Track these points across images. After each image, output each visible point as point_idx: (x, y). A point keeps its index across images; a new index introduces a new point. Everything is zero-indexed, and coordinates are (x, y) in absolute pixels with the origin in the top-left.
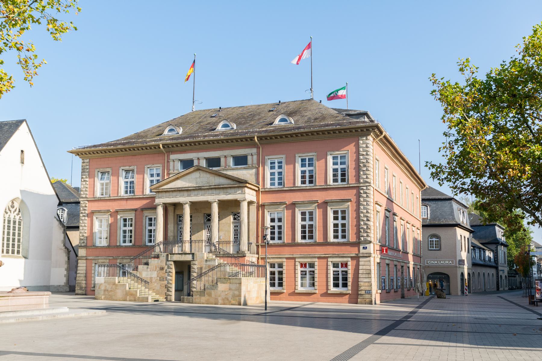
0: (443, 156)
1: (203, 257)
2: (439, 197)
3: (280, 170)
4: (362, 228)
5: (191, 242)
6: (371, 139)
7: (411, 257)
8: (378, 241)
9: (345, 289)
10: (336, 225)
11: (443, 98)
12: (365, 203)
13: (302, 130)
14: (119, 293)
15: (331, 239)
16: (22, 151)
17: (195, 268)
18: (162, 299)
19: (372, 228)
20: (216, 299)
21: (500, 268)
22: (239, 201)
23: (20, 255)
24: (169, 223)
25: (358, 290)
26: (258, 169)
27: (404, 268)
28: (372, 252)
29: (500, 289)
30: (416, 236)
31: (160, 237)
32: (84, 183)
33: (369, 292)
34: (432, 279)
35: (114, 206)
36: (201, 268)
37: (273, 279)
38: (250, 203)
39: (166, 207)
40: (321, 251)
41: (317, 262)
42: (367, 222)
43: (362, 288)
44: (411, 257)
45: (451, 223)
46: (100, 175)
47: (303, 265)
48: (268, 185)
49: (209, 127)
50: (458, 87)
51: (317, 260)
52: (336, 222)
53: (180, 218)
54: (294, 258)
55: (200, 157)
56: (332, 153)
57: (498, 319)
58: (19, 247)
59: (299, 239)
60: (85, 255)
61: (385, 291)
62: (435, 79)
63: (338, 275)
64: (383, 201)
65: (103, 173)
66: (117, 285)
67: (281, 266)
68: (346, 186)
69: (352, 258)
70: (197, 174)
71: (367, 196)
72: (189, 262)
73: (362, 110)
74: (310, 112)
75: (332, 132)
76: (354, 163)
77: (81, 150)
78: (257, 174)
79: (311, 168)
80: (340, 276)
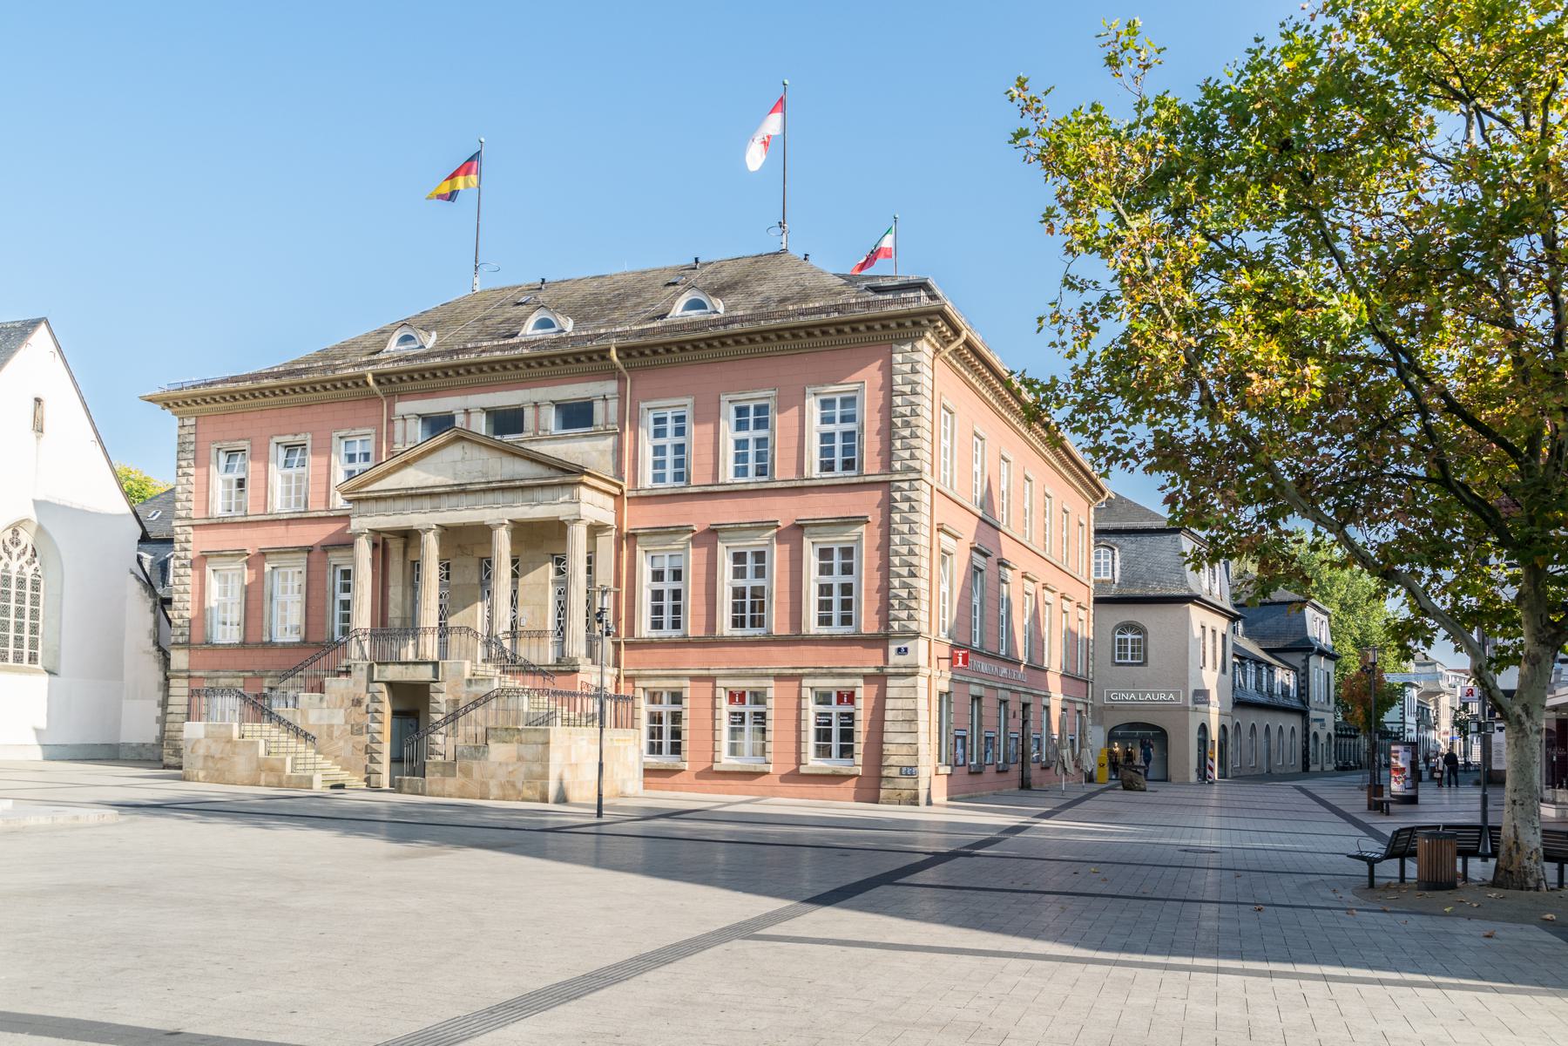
0: (1053, 345)
1: (464, 670)
2: (1147, 524)
3: (679, 440)
4: (896, 596)
5: (444, 630)
6: (929, 350)
7: (1054, 683)
8: (943, 635)
9: (846, 761)
10: (825, 590)
11: (1053, 158)
12: (905, 528)
13: (736, 327)
14: (242, 766)
15: (812, 626)
16: (38, 400)
17: (441, 702)
18: (355, 780)
19: (925, 596)
20: (484, 784)
21: (1313, 714)
22: (562, 523)
23: (39, 666)
24: (391, 583)
25: (880, 766)
26: (620, 436)
27: (1032, 708)
28: (922, 660)
29: (1313, 768)
30: (1074, 626)
31: (363, 618)
32: (184, 480)
33: (910, 772)
34: (1122, 739)
35: (254, 540)
36: (456, 702)
37: (655, 733)
38: (595, 530)
39: (381, 543)
40: (784, 658)
41: (772, 689)
42: (908, 580)
43: (892, 760)
44: (1054, 683)
45: (1176, 593)
46: (223, 458)
47: (736, 697)
48: (647, 481)
49: (503, 329)
50: (1099, 119)
51: (772, 682)
52: (826, 579)
53: (414, 570)
54: (712, 679)
55: (470, 408)
56: (819, 389)
57: (1285, 855)
58: (34, 644)
59: (725, 627)
60: (185, 666)
61: (966, 769)
62: (1026, 95)
63: (830, 723)
64: (968, 528)
65: (231, 454)
66: (235, 744)
67: (676, 698)
68: (855, 480)
69: (865, 677)
70: (455, 452)
71: (912, 509)
73: (913, 277)
74: (772, 285)
75: (817, 332)
76: (878, 416)
77: (172, 394)
78: (619, 450)
79: (762, 433)
80: (835, 729)
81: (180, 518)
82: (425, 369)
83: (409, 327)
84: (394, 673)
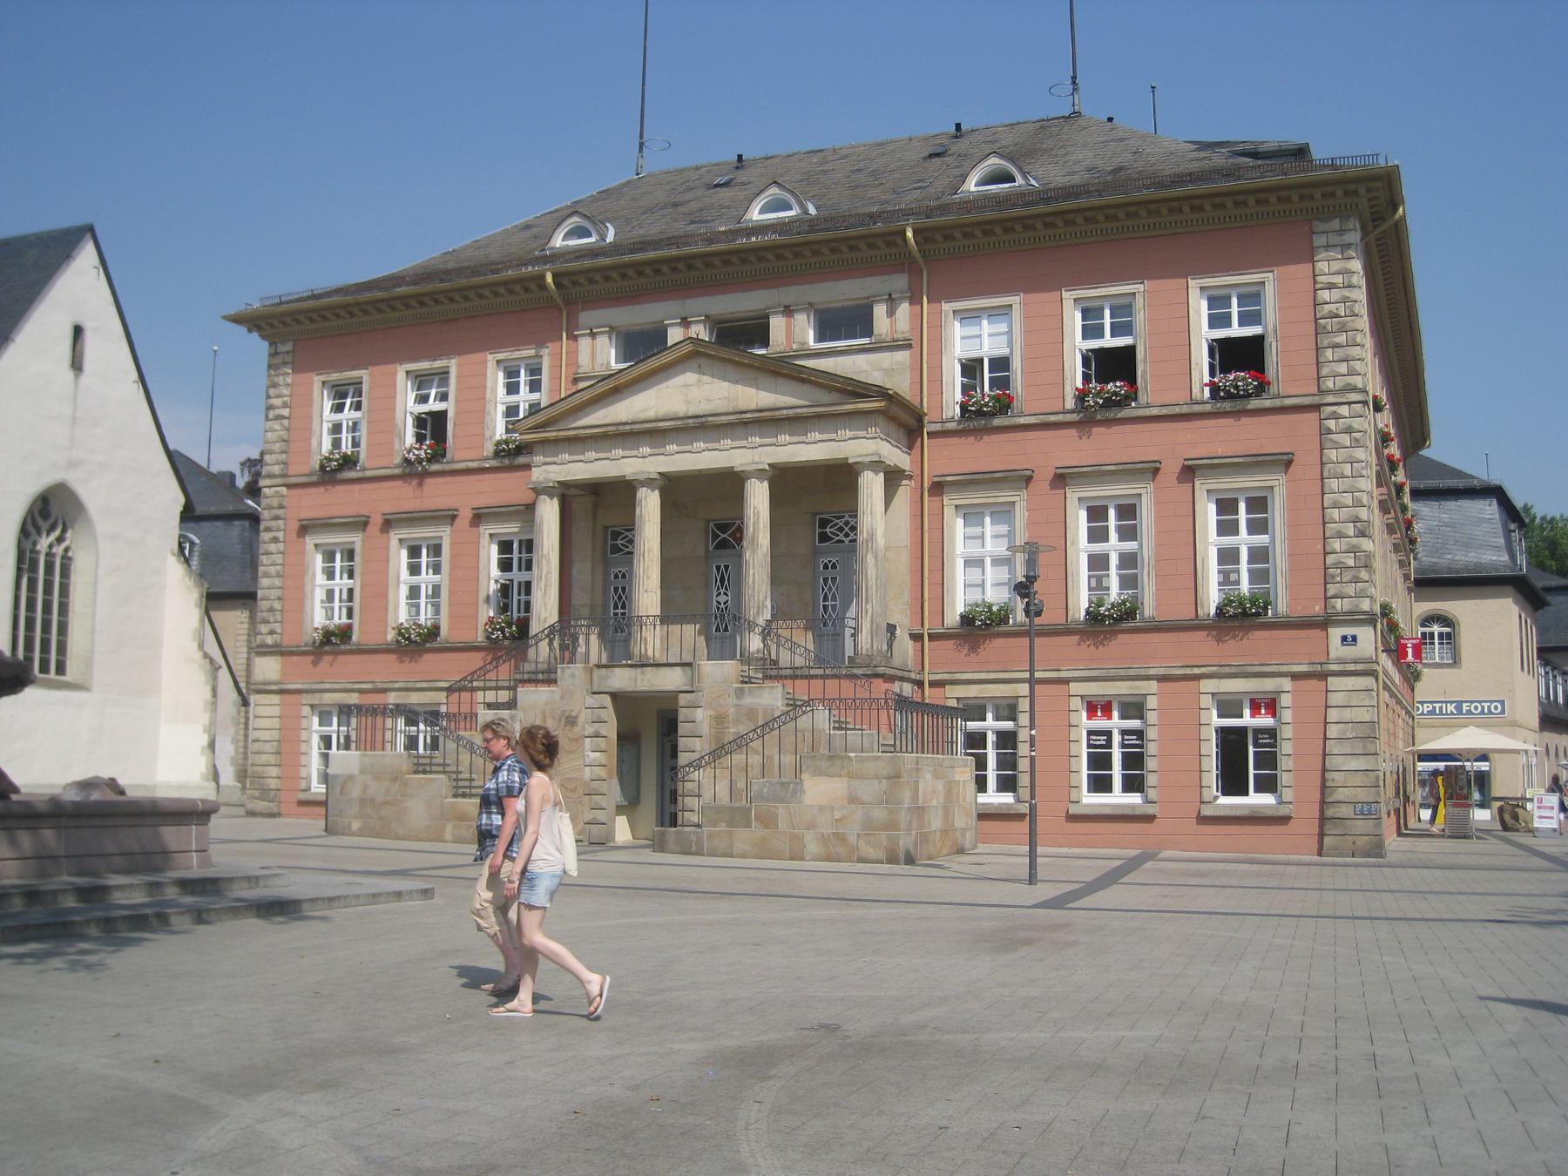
43: (1340, 794)
63: (1109, 745)
72: (673, 696)
81: (270, 476)
82: (677, 259)
83: (589, 212)
84: (622, 679)
